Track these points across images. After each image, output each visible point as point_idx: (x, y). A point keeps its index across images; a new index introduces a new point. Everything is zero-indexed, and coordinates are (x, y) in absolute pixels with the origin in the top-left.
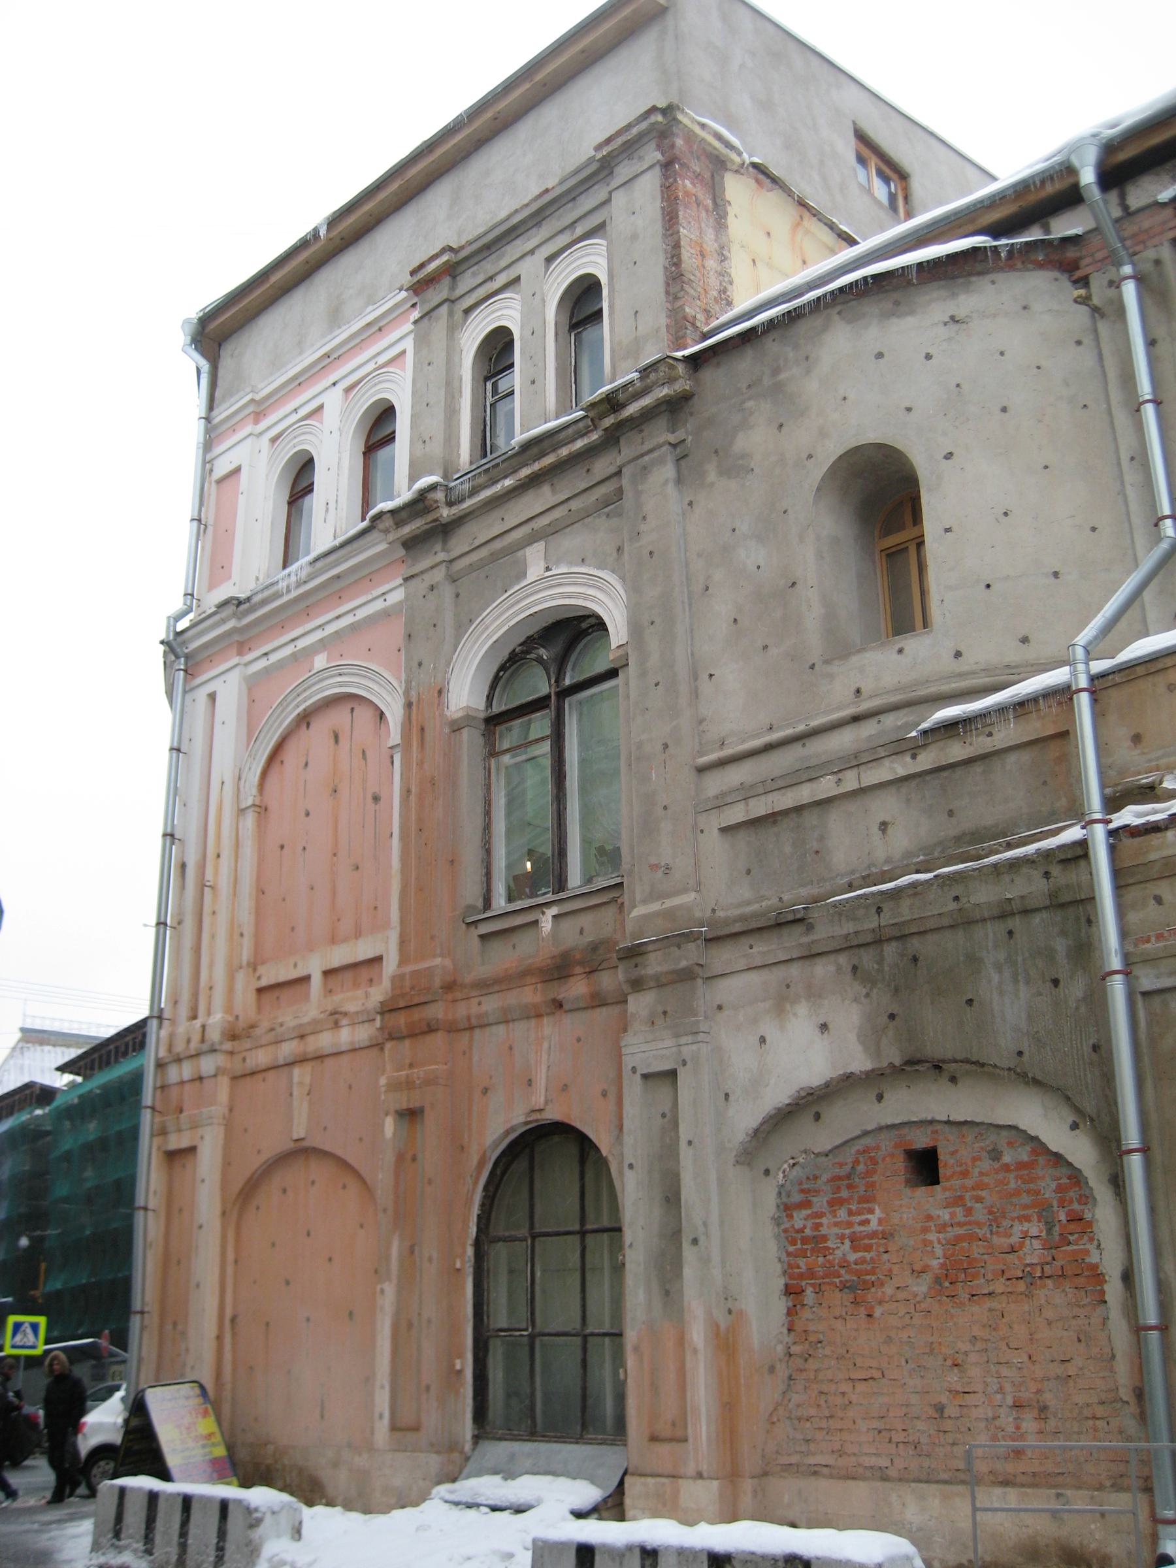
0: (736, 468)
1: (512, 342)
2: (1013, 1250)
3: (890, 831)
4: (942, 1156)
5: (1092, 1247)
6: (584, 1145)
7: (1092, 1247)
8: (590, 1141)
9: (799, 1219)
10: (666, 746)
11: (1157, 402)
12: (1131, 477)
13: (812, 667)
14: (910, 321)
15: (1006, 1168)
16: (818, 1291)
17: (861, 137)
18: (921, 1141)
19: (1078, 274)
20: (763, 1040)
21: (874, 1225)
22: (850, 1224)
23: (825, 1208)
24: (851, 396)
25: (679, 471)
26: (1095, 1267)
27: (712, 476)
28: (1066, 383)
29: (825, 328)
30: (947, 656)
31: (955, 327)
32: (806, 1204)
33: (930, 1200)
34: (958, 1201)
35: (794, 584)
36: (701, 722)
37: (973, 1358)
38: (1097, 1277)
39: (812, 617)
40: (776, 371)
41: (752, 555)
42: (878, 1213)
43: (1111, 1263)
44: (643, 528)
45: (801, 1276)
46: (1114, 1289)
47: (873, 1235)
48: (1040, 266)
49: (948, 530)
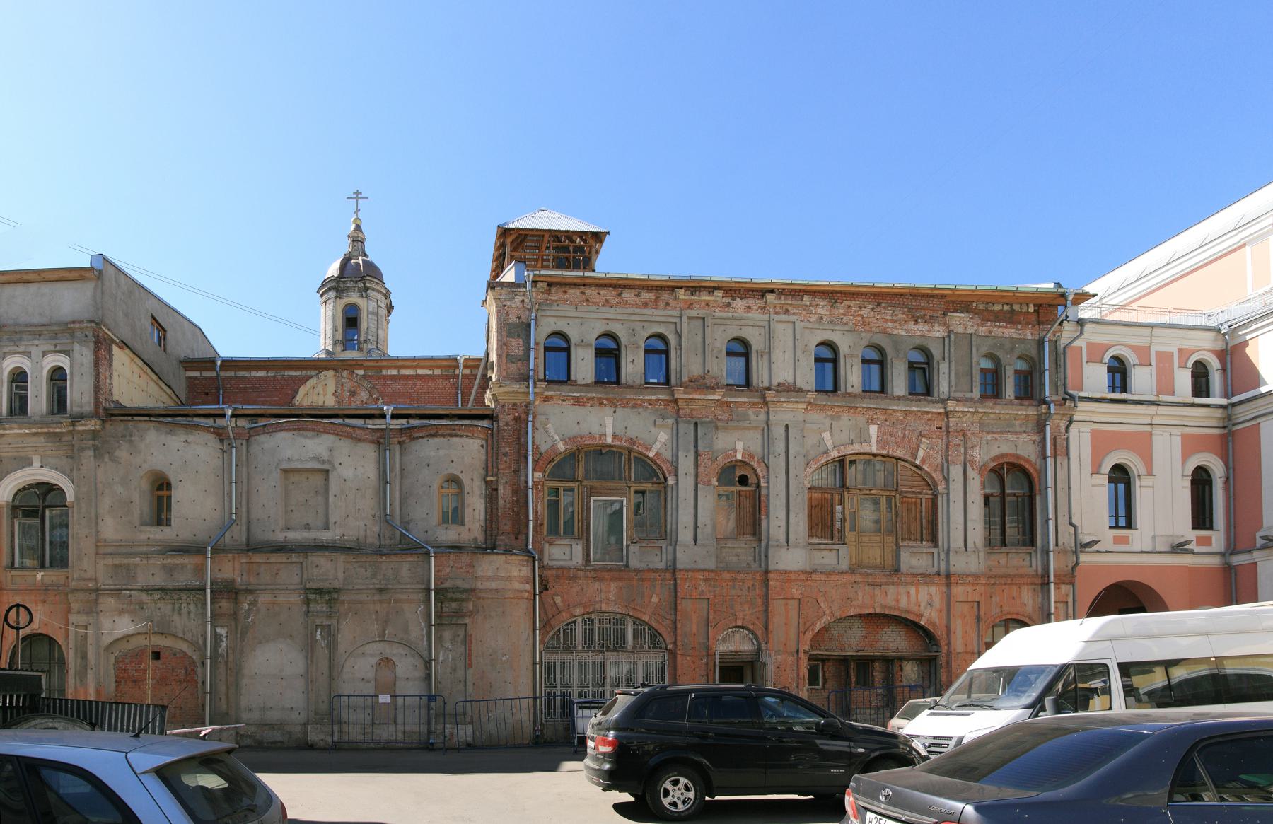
0: (114, 460)
6: (51, 641)
14: (174, 437)
16: (126, 681)
17: (153, 317)
18: (156, 650)
24: (155, 454)
27: (107, 460)
30: (174, 535)
33: (158, 663)
38: (196, 682)
39: (137, 514)
41: (120, 489)
43: (200, 681)
44: (81, 467)
46: (200, 685)
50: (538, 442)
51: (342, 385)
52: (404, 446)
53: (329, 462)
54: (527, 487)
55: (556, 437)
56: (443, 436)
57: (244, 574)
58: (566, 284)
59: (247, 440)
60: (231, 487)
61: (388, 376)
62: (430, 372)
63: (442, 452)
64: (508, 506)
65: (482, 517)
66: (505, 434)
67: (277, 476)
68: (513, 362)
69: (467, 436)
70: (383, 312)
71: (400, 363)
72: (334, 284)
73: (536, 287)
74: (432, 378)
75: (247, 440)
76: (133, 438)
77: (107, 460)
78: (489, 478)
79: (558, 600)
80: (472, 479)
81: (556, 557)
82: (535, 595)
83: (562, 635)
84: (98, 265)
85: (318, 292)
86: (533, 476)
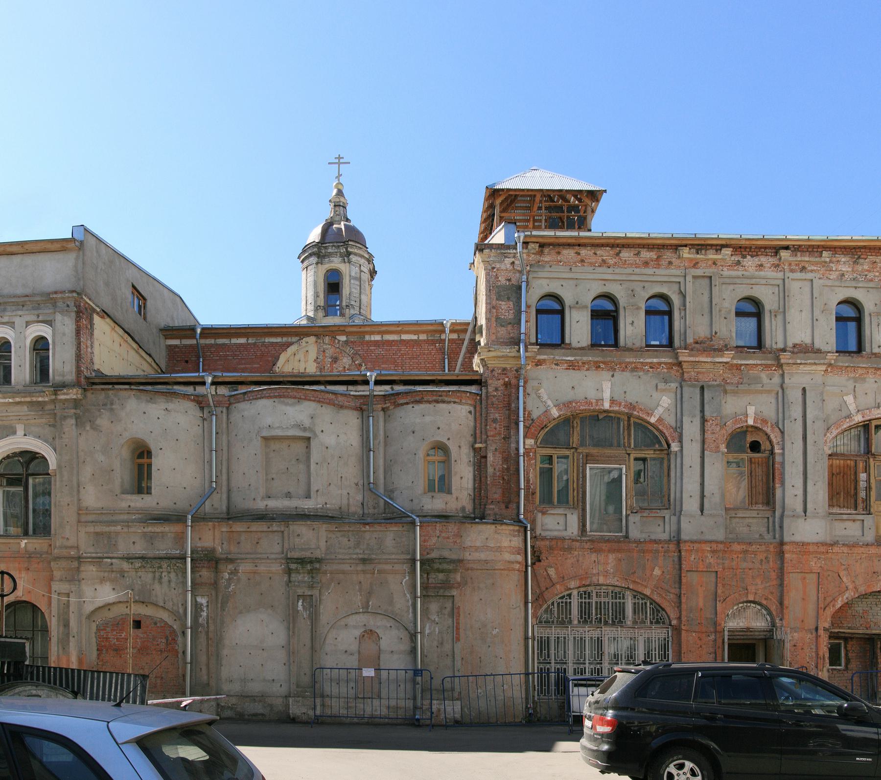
1: (11, 346)
2: (158, 645)
3: (136, 544)
4: (142, 623)
5: (177, 646)
6: (34, 608)
7: (177, 646)
8: (37, 606)
9: (102, 633)
10: (68, 504)
11: (216, 451)
12: (207, 466)
13: (117, 495)
14: (154, 406)
15: (158, 627)
17: (134, 287)
18: (137, 619)
19: (201, 405)
20: (96, 589)
21: (123, 636)
22: (117, 636)
23: (110, 631)
25: (77, 422)
26: (176, 650)
27: (88, 428)
28: (194, 437)
29: (129, 397)
31: (167, 412)
32: (105, 630)
33: (139, 632)
34: (146, 633)
35: (112, 470)
36: (80, 500)
37: (146, 667)
38: (177, 652)
39: (118, 482)
40: (112, 404)
41: (101, 458)
42: (124, 633)
44: (63, 436)
45: (102, 646)
47: (123, 638)
48: (192, 401)
49: (158, 470)
50: (529, 408)
51: (324, 351)
52: (389, 412)
53: (311, 430)
54: (518, 455)
55: (549, 403)
56: (429, 402)
57: (225, 543)
58: (559, 245)
59: (228, 408)
60: (211, 455)
61: (371, 341)
62: (415, 337)
63: (428, 419)
64: (498, 474)
65: (471, 485)
66: (494, 400)
67: (258, 443)
68: (502, 326)
69: (455, 402)
70: (366, 276)
71: (384, 329)
72: (316, 249)
73: (527, 248)
74: (417, 343)
75: (228, 408)
76: (114, 407)
77: (88, 428)
78: (477, 445)
79: (552, 572)
80: (460, 447)
81: (550, 527)
82: (527, 566)
83: (556, 609)
84: (79, 236)
85: (299, 258)
86: (524, 443)
